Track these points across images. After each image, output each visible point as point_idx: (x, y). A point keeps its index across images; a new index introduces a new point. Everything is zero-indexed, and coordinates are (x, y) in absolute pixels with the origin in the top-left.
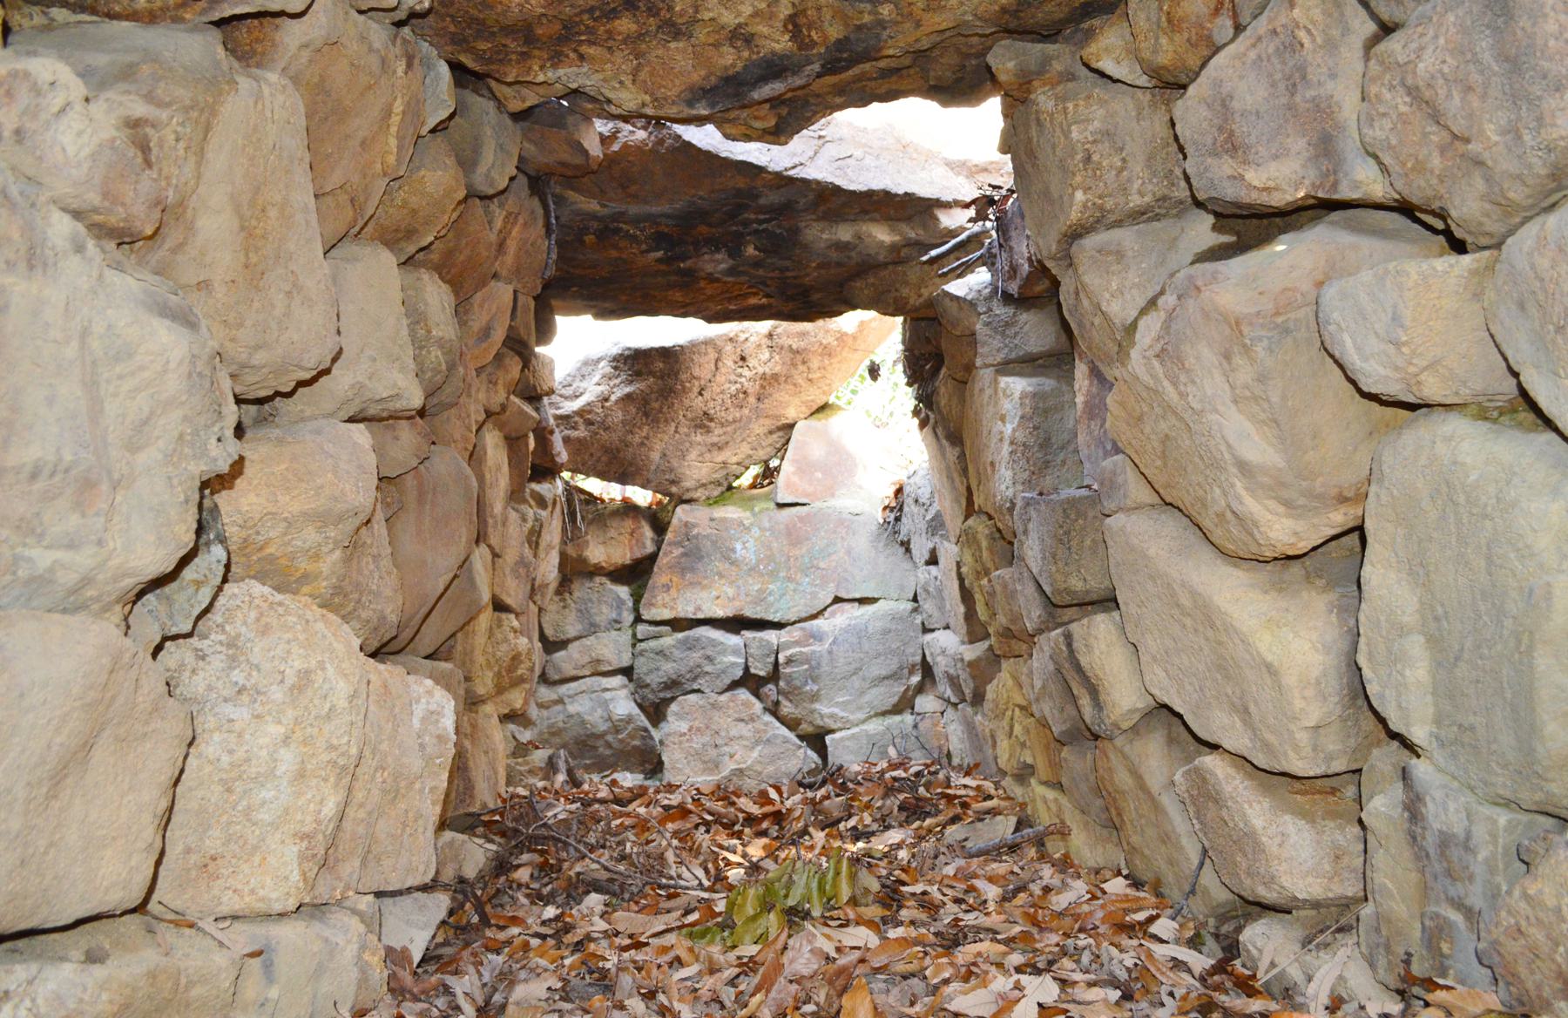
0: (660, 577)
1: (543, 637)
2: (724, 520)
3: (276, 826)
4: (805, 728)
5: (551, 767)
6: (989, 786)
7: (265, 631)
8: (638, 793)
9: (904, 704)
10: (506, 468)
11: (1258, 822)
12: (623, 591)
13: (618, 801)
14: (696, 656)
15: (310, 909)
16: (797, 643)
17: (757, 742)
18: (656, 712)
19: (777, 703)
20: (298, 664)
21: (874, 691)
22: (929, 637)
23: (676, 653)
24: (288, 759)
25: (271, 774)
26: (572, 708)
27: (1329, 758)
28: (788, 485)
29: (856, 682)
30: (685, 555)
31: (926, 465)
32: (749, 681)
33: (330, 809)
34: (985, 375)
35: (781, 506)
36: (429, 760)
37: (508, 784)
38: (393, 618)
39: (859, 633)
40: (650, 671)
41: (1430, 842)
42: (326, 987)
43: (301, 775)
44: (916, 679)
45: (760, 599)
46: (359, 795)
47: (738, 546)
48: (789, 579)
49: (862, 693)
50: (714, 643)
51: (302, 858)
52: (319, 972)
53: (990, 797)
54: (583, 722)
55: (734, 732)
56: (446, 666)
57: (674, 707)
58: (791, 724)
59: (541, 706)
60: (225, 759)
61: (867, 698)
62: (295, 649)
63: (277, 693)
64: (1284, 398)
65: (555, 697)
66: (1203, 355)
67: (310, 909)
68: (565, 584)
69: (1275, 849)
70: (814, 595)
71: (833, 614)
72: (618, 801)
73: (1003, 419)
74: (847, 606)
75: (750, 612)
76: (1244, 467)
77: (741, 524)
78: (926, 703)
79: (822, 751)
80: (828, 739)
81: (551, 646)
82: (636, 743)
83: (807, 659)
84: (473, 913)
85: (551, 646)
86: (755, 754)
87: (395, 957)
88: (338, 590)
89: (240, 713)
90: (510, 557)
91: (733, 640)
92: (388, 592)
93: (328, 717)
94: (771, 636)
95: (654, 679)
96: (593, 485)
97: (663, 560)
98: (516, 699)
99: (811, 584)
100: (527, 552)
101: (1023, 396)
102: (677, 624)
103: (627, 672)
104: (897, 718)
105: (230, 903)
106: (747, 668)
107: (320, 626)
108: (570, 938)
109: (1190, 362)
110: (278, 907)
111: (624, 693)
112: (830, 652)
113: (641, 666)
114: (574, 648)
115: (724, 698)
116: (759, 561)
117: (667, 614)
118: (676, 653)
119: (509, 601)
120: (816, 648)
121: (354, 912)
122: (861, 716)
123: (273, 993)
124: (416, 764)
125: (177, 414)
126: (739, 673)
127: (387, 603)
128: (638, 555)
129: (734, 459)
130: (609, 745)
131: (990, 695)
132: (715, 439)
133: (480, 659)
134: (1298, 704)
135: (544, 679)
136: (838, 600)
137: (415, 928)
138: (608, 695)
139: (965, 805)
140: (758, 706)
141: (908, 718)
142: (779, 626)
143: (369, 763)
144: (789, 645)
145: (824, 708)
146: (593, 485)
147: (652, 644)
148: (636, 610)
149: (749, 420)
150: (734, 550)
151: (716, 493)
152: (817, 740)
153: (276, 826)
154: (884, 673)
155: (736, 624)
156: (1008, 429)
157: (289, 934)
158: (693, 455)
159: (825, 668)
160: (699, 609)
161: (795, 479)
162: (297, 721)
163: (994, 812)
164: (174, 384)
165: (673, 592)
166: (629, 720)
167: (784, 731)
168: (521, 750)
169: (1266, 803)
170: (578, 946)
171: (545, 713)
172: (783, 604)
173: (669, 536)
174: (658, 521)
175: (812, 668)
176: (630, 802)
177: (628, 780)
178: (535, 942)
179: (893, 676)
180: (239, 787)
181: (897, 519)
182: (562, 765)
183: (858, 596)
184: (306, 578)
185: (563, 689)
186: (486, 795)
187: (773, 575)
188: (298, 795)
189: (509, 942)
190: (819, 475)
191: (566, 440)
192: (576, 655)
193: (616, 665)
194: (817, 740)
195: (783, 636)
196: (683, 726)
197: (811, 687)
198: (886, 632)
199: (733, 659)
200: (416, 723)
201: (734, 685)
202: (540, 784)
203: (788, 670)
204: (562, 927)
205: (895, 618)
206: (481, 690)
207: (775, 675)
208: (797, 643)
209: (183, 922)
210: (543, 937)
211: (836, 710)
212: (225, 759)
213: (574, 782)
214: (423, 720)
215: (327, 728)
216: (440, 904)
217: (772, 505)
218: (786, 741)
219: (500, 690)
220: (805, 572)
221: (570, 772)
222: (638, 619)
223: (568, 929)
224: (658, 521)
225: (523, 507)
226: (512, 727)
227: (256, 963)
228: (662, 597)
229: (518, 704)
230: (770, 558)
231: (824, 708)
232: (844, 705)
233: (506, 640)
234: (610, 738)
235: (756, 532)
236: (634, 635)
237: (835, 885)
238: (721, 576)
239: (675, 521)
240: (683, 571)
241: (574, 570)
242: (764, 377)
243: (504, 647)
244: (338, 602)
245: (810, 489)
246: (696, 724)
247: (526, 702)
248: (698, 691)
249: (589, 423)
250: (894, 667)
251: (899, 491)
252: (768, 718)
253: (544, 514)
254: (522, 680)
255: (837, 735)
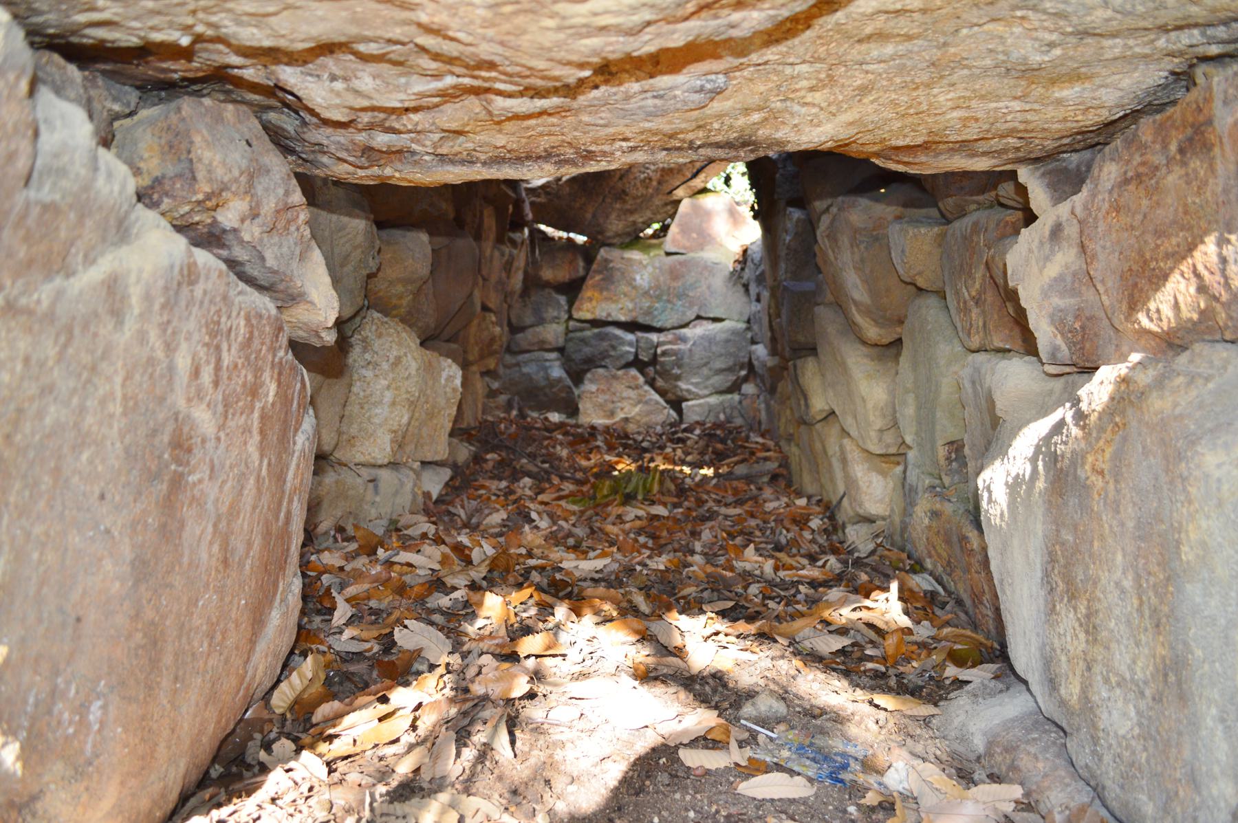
0: (587, 293)
1: (510, 324)
2: (630, 260)
3: (381, 425)
4: (670, 396)
5: (509, 406)
6: (771, 443)
7: (380, 336)
8: (561, 426)
9: (735, 388)
10: (494, 228)
11: (859, 475)
12: (563, 300)
13: (547, 430)
14: (605, 344)
15: (393, 465)
16: (670, 343)
17: (639, 402)
18: (577, 377)
19: (654, 379)
20: (395, 353)
21: (716, 378)
22: (754, 347)
23: (593, 342)
24: (388, 396)
25: (381, 402)
26: (525, 370)
27: (888, 446)
28: (674, 241)
29: (705, 371)
30: (603, 279)
31: (760, 243)
32: (637, 363)
33: (405, 420)
34: (782, 204)
35: (668, 254)
36: (448, 400)
37: (483, 413)
38: (433, 326)
39: (709, 340)
40: (576, 351)
41: (907, 487)
42: (399, 500)
43: (393, 404)
44: (743, 373)
45: (648, 312)
46: (417, 415)
47: (638, 277)
48: (669, 301)
49: (708, 378)
50: (617, 337)
51: (392, 441)
52: (396, 493)
53: (769, 450)
54: (531, 379)
55: (625, 394)
56: (454, 346)
57: (589, 375)
58: (662, 393)
59: (505, 366)
60: (362, 394)
61: (711, 381)
62: (394, 345)
63: (385, 366)
64: (872, 271)
65: (514, 361)
66: (845, 241)
67: (393, 465)
68: (525, 292)
69: (865, 489)
70: (684, 313)
71: (695, 326)
72: (547, 430)
73: (786, 232)
74: (705, 322)
75: (641, 320)
76: (856, 303)
77: (641, 263)
78: (749, 388)
79: (680, 411)
80: (684, 405)
81: (515, 329)
82: (563, 395)
83: (675, 353)
84: (462, 480)
85: (515, 329)
86: (637, 409)
87: (427, 495)
88: (409, 313)
89: (369, 374)
90: (494, 279)
91: (630, 337)
92: (431, 312)
93: (407, 378)
94: (654, 337)
95: (577, 357)
96: (549, 230)
97: (589, 282)
98: (491, 363)
99: (683, 306)
100: (504, 275)
101: (798, 220)
102: (595, 323)
103: (561, 350)
104: (729, 396)
105: (360, 458)
106: (636, 355)
107: (404, 335)
108: (512, 497)
109: (840, 243)
110: (380, 462)
111: (557, 363)
112: (690, 350)
113: (571, 347)
114: (530, 332)
115: (620, 373)
116: (650, 288)
117: (588, 316)
118: (593, 342)
119: (491, 305)
120: (682, 346)
121: (411, 469)
122: (706, 392)
123: (378, 499)
124: (442, 402)
125: (359, 251)
126: (631, 358)
127: (430, 320)
128: (574, 276)
129: (641, 220)
130: (545, 395)
131: (779, 389)
132: (628, 207)
133: (472, 340)
134: (872, 418)
135: (509, 350)
136: (699, 317)
137: (434, 483)
138: (548, 364)
139: (753, 453)
140: (641, 379)
141: (736, 397)
142: (660, 330)
143: (423, 399)
144: (664, 343)
145: (683, 385)
146: (549, 230)
147: (579, 334)
148: (569, 312)
149: (652, 196)
150: (635, 280)
151: (627, 240)
152: (676, 404)
153: (381, 425)
154: (723, 366)
155: (632, 326)
156: (788, 238)
157: (385, 475)
158: (613, 216)
159: (686, 360)
160: (609, 315)
161: (679, 237)
162: (394, 379)
163: (766, 459)
164: (360, 239)
165: (594, 303)
166: (560, 380)
167: (657, 397)
168: (492, 394)
169: (866, 465)
170: (515, 502)
171: (508, 371)
172: (663, 317)
173: (594, 266)
174: (588, 253)
175: (678, 359)
176: (554, 431)
177: (555, 417)
178: (493, 498)
179: (729, 370)
180: (366, 406)
181: (743, 269)
182: (515, 405)
183: (712, 316)
184: (395, 307)
185: (521, 358)
186: (469, 420)
187: (659, 298)
188: (392, 412)
189: (480, 496)
190: (694, 235)
191: (532, 204)
192: (530, 337)
193: (554, 345)
194: (676, 404)
195: (662, 337)
196: (593, 388)
197: (676, 371)
198: (727, 341)
199: (628, 348)
200: (443, 381)
201: (628, 365)
202: (502, 415)
203: (662, 359)
204: (509, 492)
205: (735, 332)
206: (471, 358)
207: (654, 360)
208: (670, 343)
209: (341, 464)
210: (498, 496)
211: (691, 387)
212: (362, 394)
213: (522, 415)
214: (447, 380)
215: (406, 383)
216: (446, 474)
217: (662, 253)
218: (657, 403)
219: (482, 357)
220: (679, 297)
221: (520, 410)
222: (570, 318)
223: (512, 492)
224: (588, 253)
225: (503, 247)
226: (487, 379)
227: (371, 485)
228: (587, 305)
229: (492, 367)
230: (658, 287)
231: (683, 385)
232: (696, 385)
233: (487, 328)
234: (547, 390)
235: (650, 269)
236: (567, 327)
237: (652, 484)
238: (625, 295)
239: (599, 257)
240: (601, 291)
241: (532, 283)
242: (663, 169)
243: (486, 333)
244: (407, 320)
245: (688, 244)
246: (602, 387)
247: (497, 364)
248: (604, 367)
249: (547, 194)
250: (731, 363)
251: (745, 251)
252: (647, 388)
253: (515, 252)
254: (495, 352)
255: (690, 403)
